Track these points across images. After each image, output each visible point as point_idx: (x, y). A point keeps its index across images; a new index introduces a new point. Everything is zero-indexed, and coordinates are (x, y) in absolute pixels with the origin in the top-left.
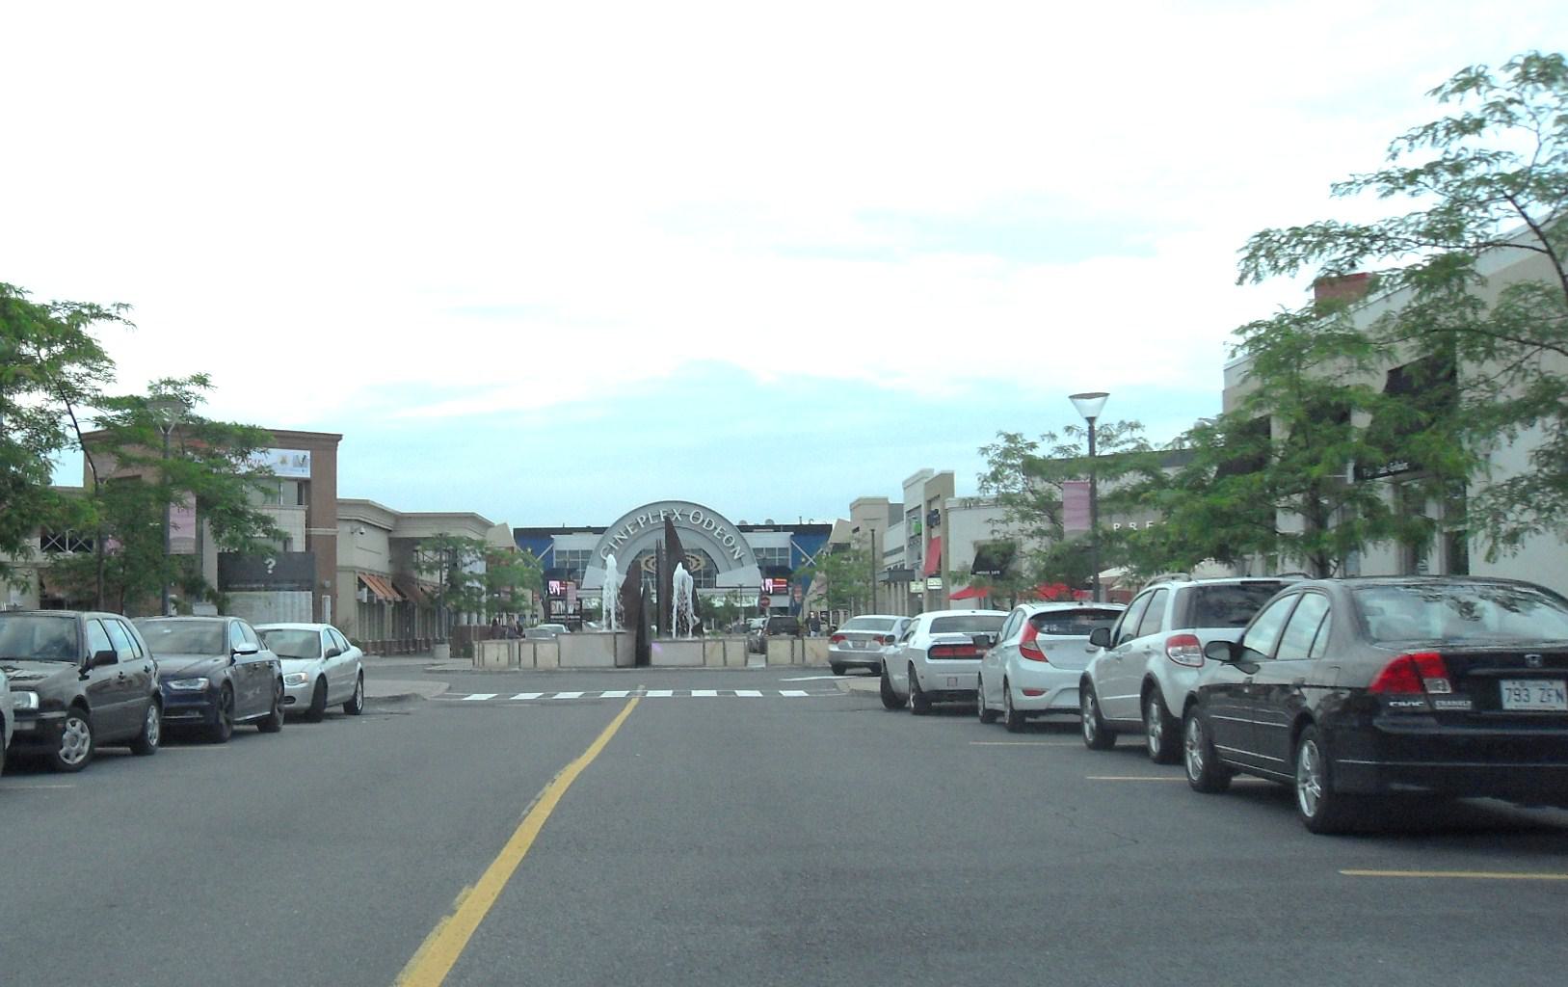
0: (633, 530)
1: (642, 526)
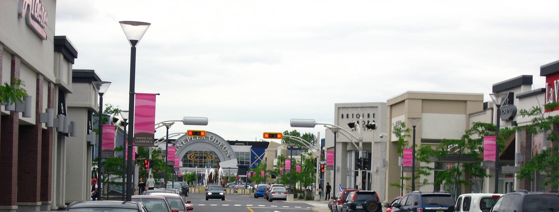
0: (185, 143)
1: (189, 141)
